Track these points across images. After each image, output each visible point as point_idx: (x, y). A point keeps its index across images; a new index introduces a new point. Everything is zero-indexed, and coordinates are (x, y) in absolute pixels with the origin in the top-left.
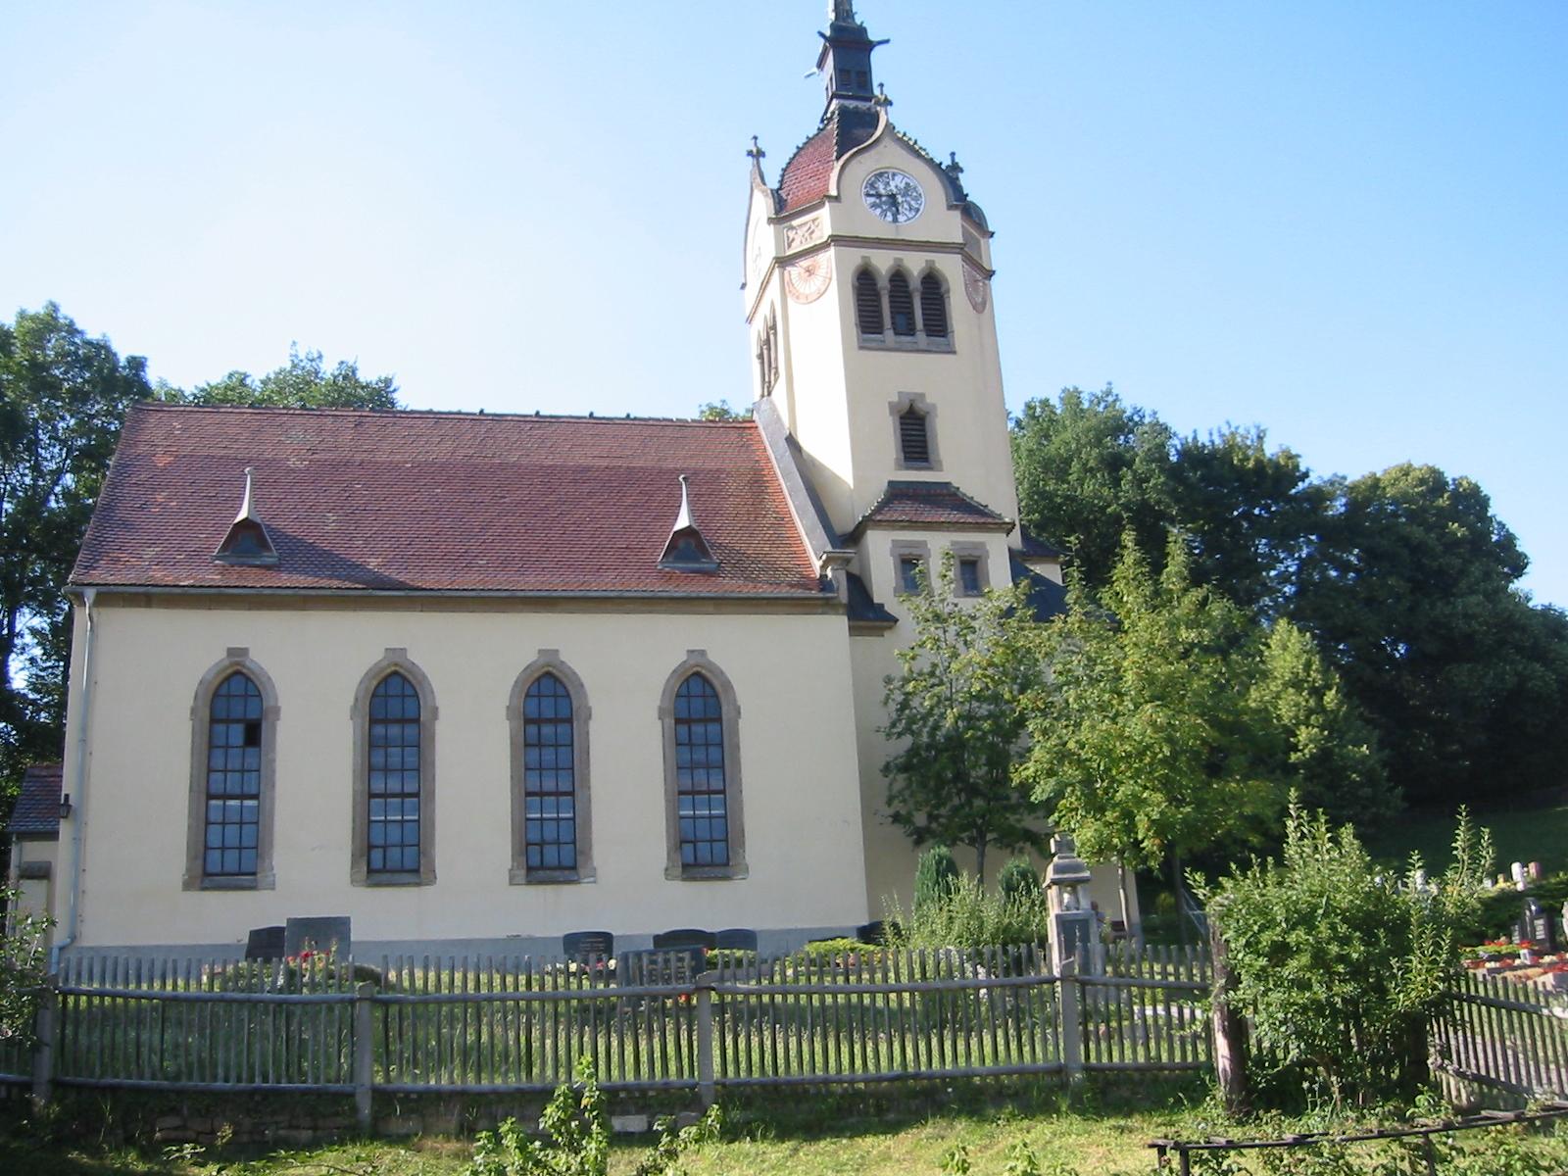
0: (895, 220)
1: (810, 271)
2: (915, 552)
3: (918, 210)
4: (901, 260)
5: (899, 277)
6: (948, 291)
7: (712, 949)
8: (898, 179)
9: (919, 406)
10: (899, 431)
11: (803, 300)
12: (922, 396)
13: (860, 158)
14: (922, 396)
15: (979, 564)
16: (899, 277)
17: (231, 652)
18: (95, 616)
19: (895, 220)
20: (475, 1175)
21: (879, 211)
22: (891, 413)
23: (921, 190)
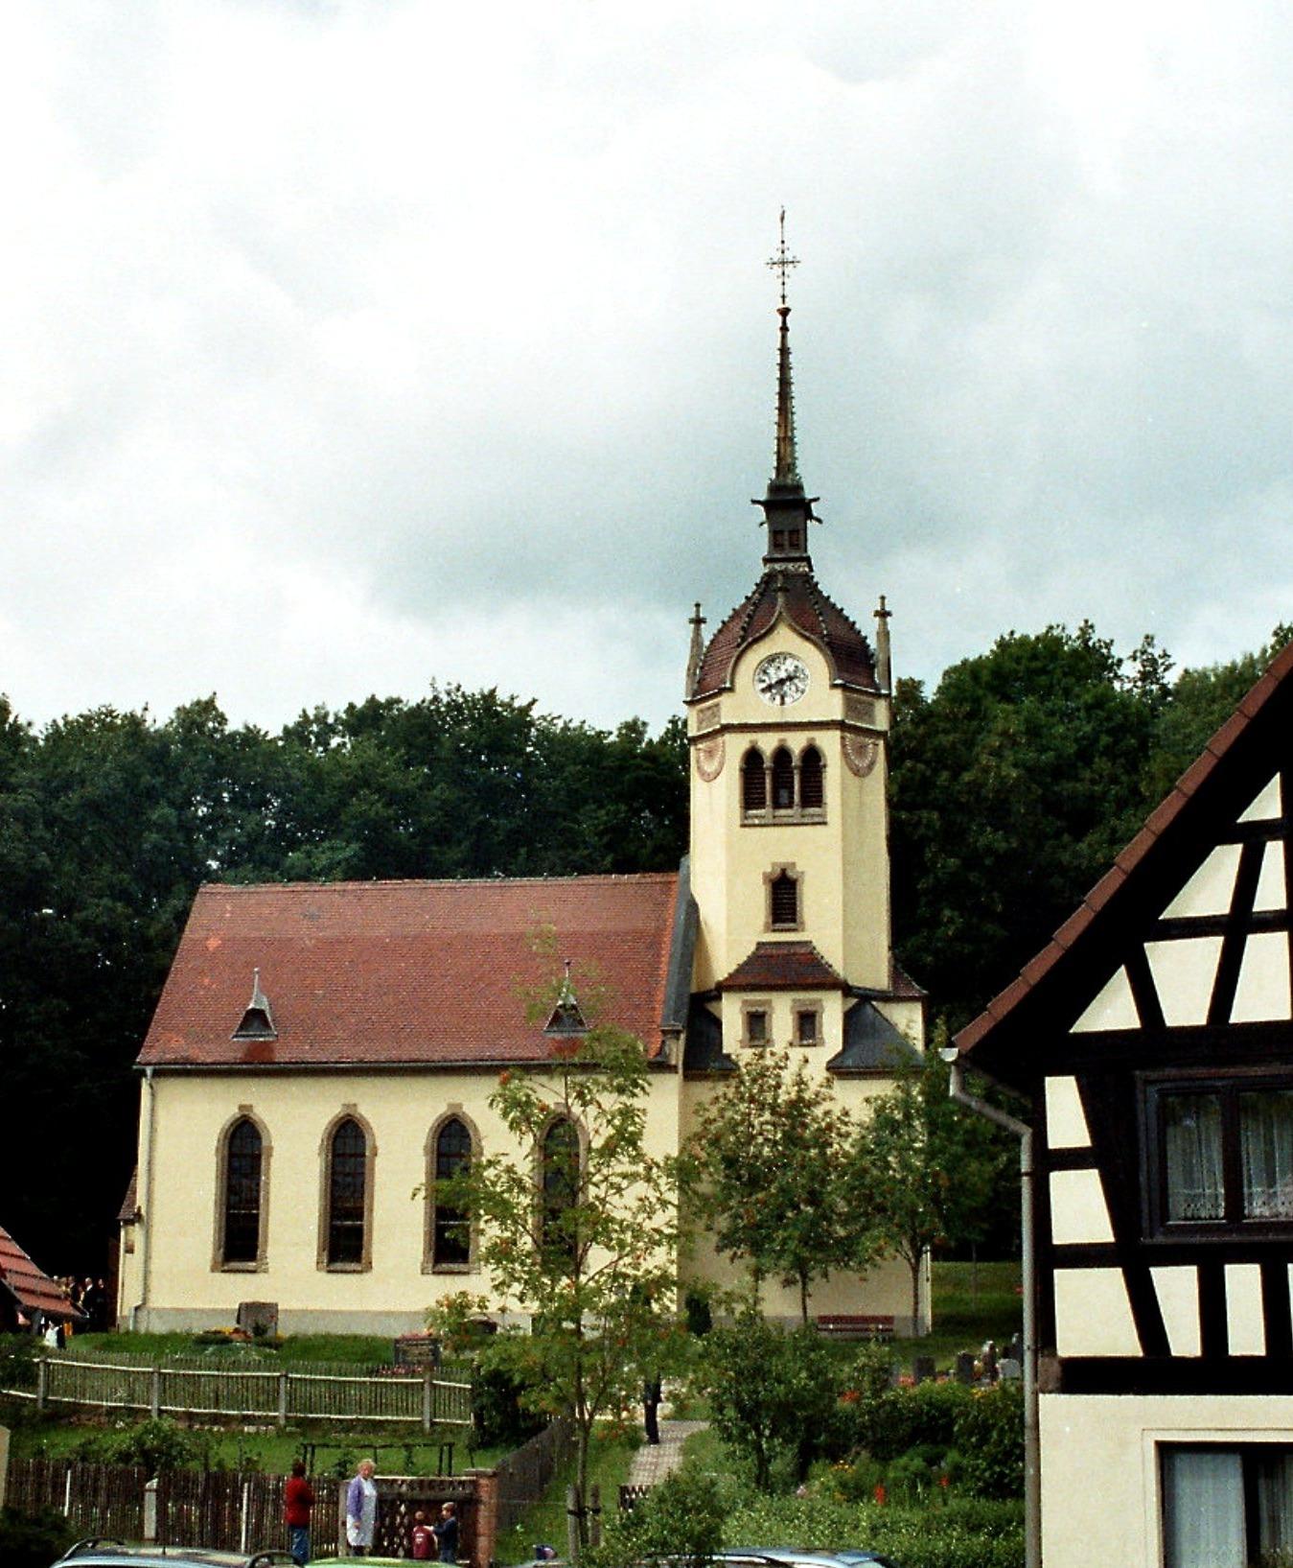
0: (783, 703)
1: (710, 753)
2: (761, 1009)
3: (803, 692)
4: (813, 739)
5: (782, 754)
6: (825, 766)
7: (964, 1355)
8: (789, 661)
9: (790, 873)
10: (798, 896)
11: (706, 777)
12: (794, 864)
13: (755, 647)
14: (794, 864)
15: (767, 1017)
16: (782, 754)
17: (450, 1106)
18: (154, 1085)
19: (783, 703)
20: (673, 1567)
21: (768, 695)
22: (764, 883)
23: (807, 672)
